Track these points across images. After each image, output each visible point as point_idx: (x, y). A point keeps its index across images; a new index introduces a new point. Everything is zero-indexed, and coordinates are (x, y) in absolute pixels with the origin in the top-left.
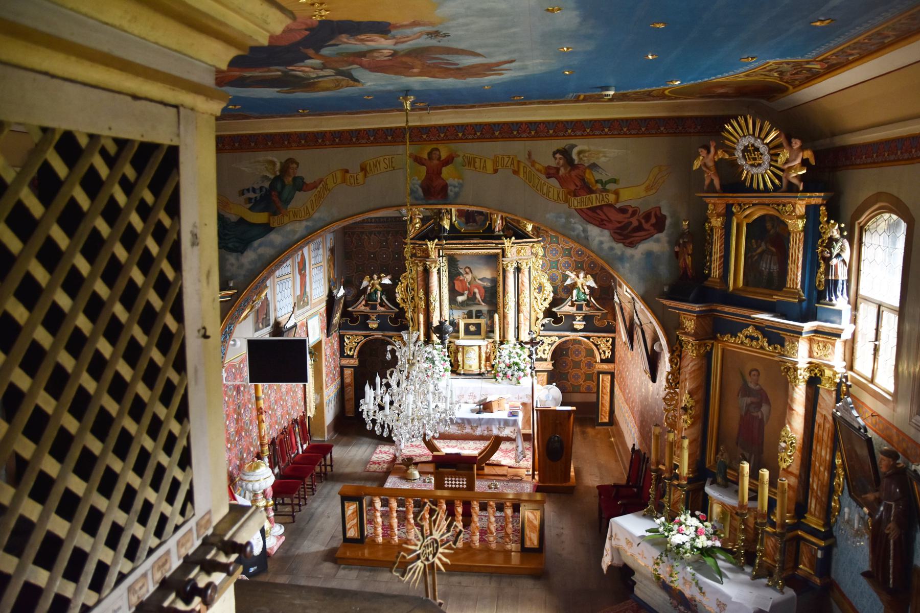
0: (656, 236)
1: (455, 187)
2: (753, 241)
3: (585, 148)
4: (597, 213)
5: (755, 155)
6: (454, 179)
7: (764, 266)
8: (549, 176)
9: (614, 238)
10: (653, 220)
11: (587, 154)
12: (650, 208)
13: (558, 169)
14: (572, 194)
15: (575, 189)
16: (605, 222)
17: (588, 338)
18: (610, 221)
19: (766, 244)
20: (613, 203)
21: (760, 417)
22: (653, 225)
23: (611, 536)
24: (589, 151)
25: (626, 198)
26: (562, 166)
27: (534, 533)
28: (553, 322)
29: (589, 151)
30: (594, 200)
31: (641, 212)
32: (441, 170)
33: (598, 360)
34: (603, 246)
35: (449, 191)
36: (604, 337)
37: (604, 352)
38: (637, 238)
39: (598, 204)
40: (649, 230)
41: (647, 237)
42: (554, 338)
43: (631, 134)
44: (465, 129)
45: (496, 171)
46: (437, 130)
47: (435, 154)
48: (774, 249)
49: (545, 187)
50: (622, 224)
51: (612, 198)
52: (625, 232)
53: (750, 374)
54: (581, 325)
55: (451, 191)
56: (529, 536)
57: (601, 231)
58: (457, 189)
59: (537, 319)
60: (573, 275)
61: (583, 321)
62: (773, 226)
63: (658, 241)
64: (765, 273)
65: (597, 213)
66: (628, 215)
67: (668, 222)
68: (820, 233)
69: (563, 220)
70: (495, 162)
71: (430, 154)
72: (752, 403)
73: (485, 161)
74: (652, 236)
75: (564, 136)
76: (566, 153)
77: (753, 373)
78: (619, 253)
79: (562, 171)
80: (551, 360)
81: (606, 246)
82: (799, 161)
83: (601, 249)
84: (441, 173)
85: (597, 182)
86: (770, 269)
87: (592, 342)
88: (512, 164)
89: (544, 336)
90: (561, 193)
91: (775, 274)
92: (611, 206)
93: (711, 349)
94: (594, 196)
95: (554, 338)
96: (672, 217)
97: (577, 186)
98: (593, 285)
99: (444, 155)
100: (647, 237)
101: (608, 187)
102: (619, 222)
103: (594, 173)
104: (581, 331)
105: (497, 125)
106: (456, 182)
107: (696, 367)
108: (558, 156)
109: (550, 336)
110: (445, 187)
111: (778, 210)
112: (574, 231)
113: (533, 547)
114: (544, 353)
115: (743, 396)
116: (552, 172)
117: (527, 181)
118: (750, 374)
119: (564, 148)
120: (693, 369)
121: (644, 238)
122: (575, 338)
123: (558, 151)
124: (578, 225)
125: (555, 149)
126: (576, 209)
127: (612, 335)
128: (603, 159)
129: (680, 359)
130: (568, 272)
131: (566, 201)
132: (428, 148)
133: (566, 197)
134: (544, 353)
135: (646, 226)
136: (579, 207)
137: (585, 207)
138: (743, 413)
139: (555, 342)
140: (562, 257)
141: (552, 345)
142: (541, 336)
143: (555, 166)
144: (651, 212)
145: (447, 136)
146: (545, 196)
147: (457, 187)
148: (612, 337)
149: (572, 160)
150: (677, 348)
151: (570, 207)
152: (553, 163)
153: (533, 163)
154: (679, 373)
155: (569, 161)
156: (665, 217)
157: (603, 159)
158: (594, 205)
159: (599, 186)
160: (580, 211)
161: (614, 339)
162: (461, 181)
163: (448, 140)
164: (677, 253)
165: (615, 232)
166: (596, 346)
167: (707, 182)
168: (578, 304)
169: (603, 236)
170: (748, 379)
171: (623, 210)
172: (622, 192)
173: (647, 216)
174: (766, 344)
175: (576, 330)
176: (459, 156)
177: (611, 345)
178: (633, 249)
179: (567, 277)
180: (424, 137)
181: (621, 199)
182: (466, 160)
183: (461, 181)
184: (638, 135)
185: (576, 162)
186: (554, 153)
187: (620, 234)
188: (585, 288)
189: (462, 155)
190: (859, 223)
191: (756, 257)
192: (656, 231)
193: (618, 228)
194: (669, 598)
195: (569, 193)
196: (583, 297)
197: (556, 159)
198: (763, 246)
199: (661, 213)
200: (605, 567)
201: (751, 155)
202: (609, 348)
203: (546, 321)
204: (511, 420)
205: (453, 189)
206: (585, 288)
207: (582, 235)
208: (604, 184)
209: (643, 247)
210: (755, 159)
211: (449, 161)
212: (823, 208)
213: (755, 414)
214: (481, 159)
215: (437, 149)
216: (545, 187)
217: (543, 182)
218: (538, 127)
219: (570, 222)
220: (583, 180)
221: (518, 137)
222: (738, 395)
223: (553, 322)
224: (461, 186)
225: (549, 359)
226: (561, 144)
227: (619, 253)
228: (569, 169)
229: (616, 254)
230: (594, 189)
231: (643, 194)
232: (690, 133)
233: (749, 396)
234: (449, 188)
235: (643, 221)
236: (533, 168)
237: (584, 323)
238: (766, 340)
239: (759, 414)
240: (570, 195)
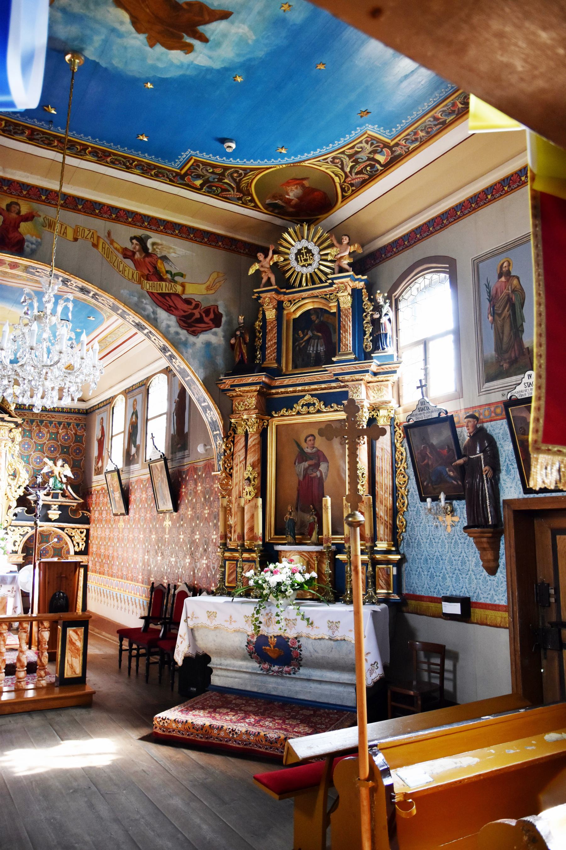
0: (214, 330)
1: (32, 243)
2: (300, 332)
3: (158, 241)
4: (166, 299)
5: (307, 256)
6: (32, 236)
7: (311, 349)
8: (125, 257)
9: (180, 325)
10: (212, 316)
11: (160, 247)
12: (209, 305)
13: (134, 253)
14: (145, 278)
15: (148, 274)
16: (172, 308)
17: (63, 529)
18: (177, 309)
19: (312, 332)
20: (180, 293)
21: (319, 476)
22: (211, 320)
23: (187, 618)
24: (161, 245)
25: (191, 292)
26: (138, 251)
27: (76, 658)
28: (27, 512)
29: (161, 245)
30: (164, 287)
31: (202, 307)
32: (19, 224)
33: (72, 552)
34: (170, 329)
35: (25, 246)
36: (78, 529)
37: (78, 544)
38: (198, 329)
39: (167, 292)
40: (208, 324)
41: (207, 328)
42: (26, 529)
43: (196, 240)
44: (49, 194)
45: (76, 240)
46: (20, 186)
47: (14, 207)
48: (319, 334)
49: (122, 265)
50: (187, 313)
51: (179, 289)
52: (189, 321)
53: (306, 440)
54: (56, 514)
55: (27, 246)
56: (70, 662)
57: (169, 316)
58: (34, 246)
59: (10, 507)
60: (50, 463)
61: (59, 510)
62: (318, 317)
63: (215, 334)
64: (313, 355)
65: (166, 299)
66: (192, 307)
67: (224, 319)
68: (364, 309)
69: (136, 299)
70: (76, 231)
71: (9, 206)
72: (310, 466)
73: (66, 227)
74: (211, 329)
75: (141, 226)
76: (142, 241)
77: (309, 439)
78: (183, 339)
79: (138, 256)
80: (22, 553)
81: (173, 330)
82: (347, 253)
83: (168, 332)
84: (19, 227)
85: (167, 272)
86: (317, 350)
87: (67, 533)
88: (92, 237)
89: (16, 526)
90: (135, 275)
91: (322, 354)
92: (178, 295)
93: (267, 426)
94: (164, 283)
95: (26, 529)
96: (227, 316)
97: (150, 272)
98: (70, 475)
99: (24, 210)
100: (207, 328)
101: (176, 278)
102: (185, 311)
103: (165, 264)
104: (55, 521)
105: (80, 200)
106: (34, 239)
107: (256, 441)
108: (135, 241)
109: (22, 526)
110: (21, 241)
111: (326, 299)
112: (144, 311)
113: (75, 676)
114: (15, 545)
115: (300, 463)
116: (129, 254)
117: (105, 256)
118: (306, 440)
119: (141, 237)
120: (254, 443)
121: (204, 329)
122: (49, 528)
123: (135, 238)
124: (149, 308)
125: (133, 236)
126: (148, 292)
127: (87, 526)
128: (173, 255)
129: (234, 445)
130: (46, 460)
131: (140, 282)
132: (8, 200)
133: (140, 279)
134: (15, 545)
135: (206, 319)
136: (150, 291)
137: (156, 291)
138: (301, 478)
139: (27, 532)
140: (34, 452)
141: (23, 536)
142: (12, 526)
143: (132, 249)
144: (210, 309)
145: (30, 195)
146: (121, 273)
147: (35, 244)
148: (86, 529)
149: (147, 249)
150: (230, 434)
151: (142, 288)
152: (130, 246)
153: (112, 242)
154: (232, 459)
155: (144, 248)
156: (221, 315)
157: (173, 255)
158: (164, 291)
159: (169, 276)
160: (151, 294)
161: (88, 530)
162: (39, 240)
163: (31, 198)
164: (232, 346)
165: (180, 319)
166: (71, 537)
167: (264, 280)
168: (53, 493)
169: (170, 320)
170: (304, 445)
171: (188, 302)
172: (187, 286)
173: (207, 311)
174: (323, 407)
175: (50, 520)
176: (40, 216)
177: (85, 536)
178: (195, 337)
179: (45, 464)
180: (5, 188)
181: (186, 292)
182: (47, 222)
183: (39, 240)
184: (201, 242)
185: (150, 251)
186: (132, 239)
187: (184, 322)
188: (62, 476)
189: (43, 216)
190: (395, 296)
191: (303, 344)
192: (214, 326)
193: (183, 316)
194: (258, 665)
195: (143, 276)
196: (59, 485)
197: (132, 243)
198: (310, 334)
199: (218, 312)
200: (179, 658)
201: (303, 257)
202: (83, 539)
203: (19, 510)
204: (10, 576)
205: (30, 245)
206: (62, 476)
207: (152, 316)
208: (173, 275)
209: (203, 337)
210: (306, 260)
211: (29, 218)
212: (364, 291)
213: (314, 475)
214: (62, 225)
215: (17, 204)
216: (122, 265)
217: (120, 260)
218: (119, 212)
219: (142, 302)
220: (155, 267)
221: (99, 216)
222: (295, 464)
223: (27, 512)
224: (39, 244)
225: (20, 551)
226: (139, 232)
227: (183, 339)
228: (143, 255)
229: (181, 339)
230: (165, 277)
231: (205, 292)
232: (241, 252)
233: (306, 461)
234: (26, 244)
235: (204, 315)
236: (112, 246)
237: (60, 512)
238: (322, 403)
239: (318, 473)
240: (143, 278)
